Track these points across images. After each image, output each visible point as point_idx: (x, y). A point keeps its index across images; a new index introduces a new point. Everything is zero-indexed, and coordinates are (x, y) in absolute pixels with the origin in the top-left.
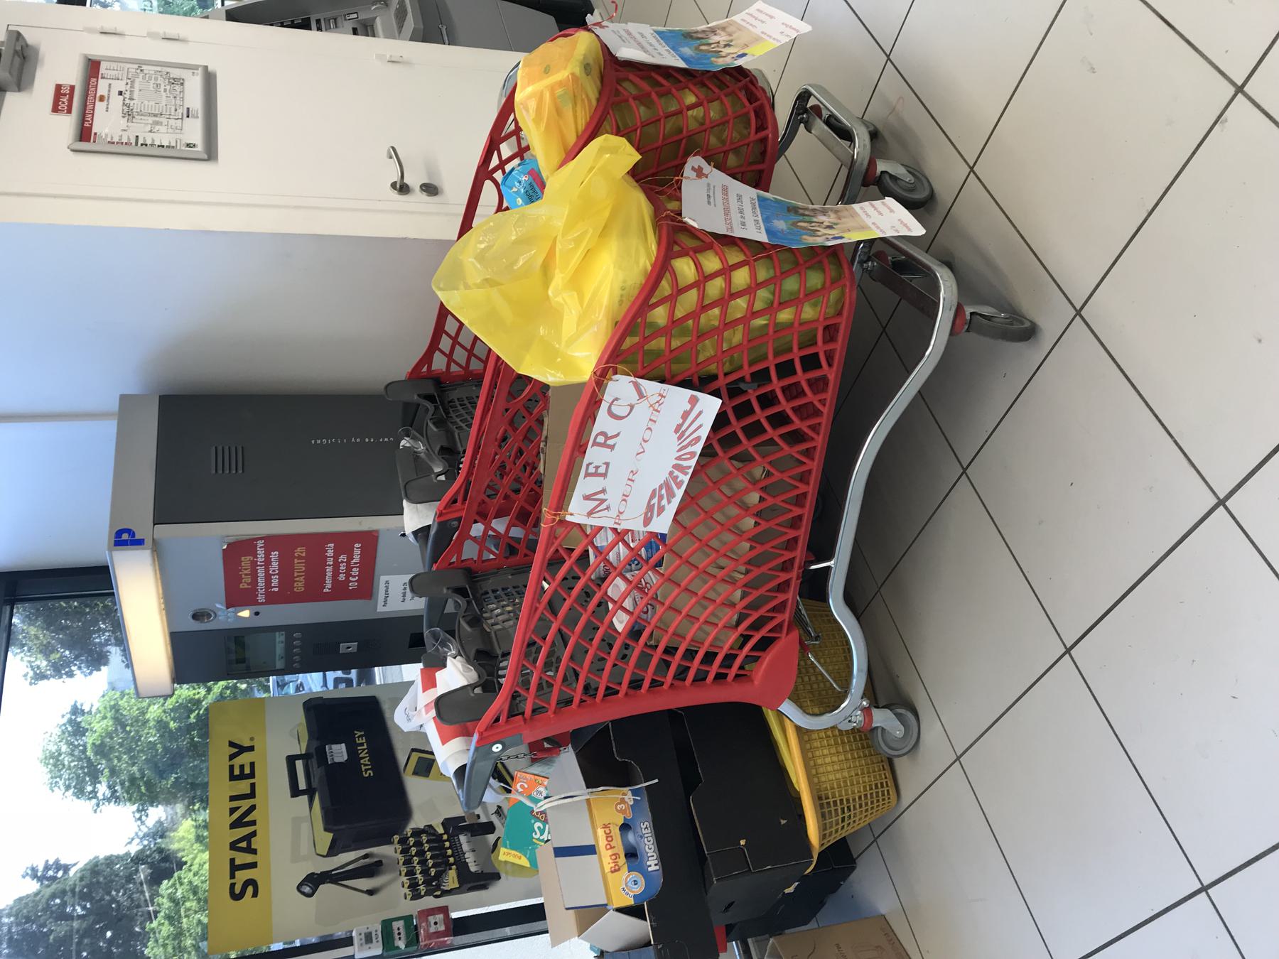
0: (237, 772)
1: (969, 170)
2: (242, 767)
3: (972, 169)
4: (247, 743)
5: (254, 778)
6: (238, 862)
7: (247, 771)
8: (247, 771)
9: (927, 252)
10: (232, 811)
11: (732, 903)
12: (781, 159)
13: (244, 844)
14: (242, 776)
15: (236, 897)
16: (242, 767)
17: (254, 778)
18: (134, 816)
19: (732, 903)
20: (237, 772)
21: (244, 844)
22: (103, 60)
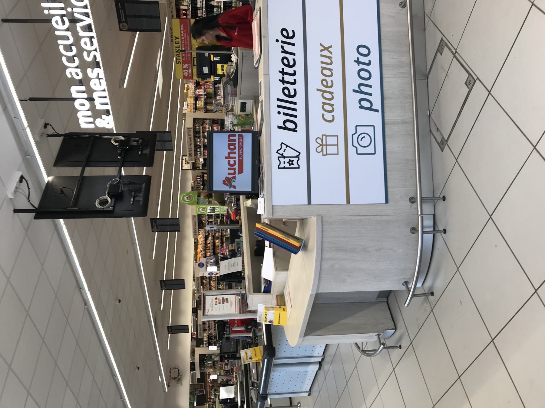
0: (176, 42)
1: (534, 3)
2: (177, 41)
3: (490, 93)
4: (177, 37)
5: (229, 143)
6: (177, 58)
7: (178, 42)
8: (178, 42)
9: (351, 343)
10: (176, 49)
11: (461, 305)
12: (320, 92)
13: (178, 55)
14: (177, 43)
15: (178, 64)
16: (177, 41)
17: (229, 143)
18: (194, 93)
19: (461, 305)
20: (176, 42)
21: (178, 55)
22: (272, 204)
